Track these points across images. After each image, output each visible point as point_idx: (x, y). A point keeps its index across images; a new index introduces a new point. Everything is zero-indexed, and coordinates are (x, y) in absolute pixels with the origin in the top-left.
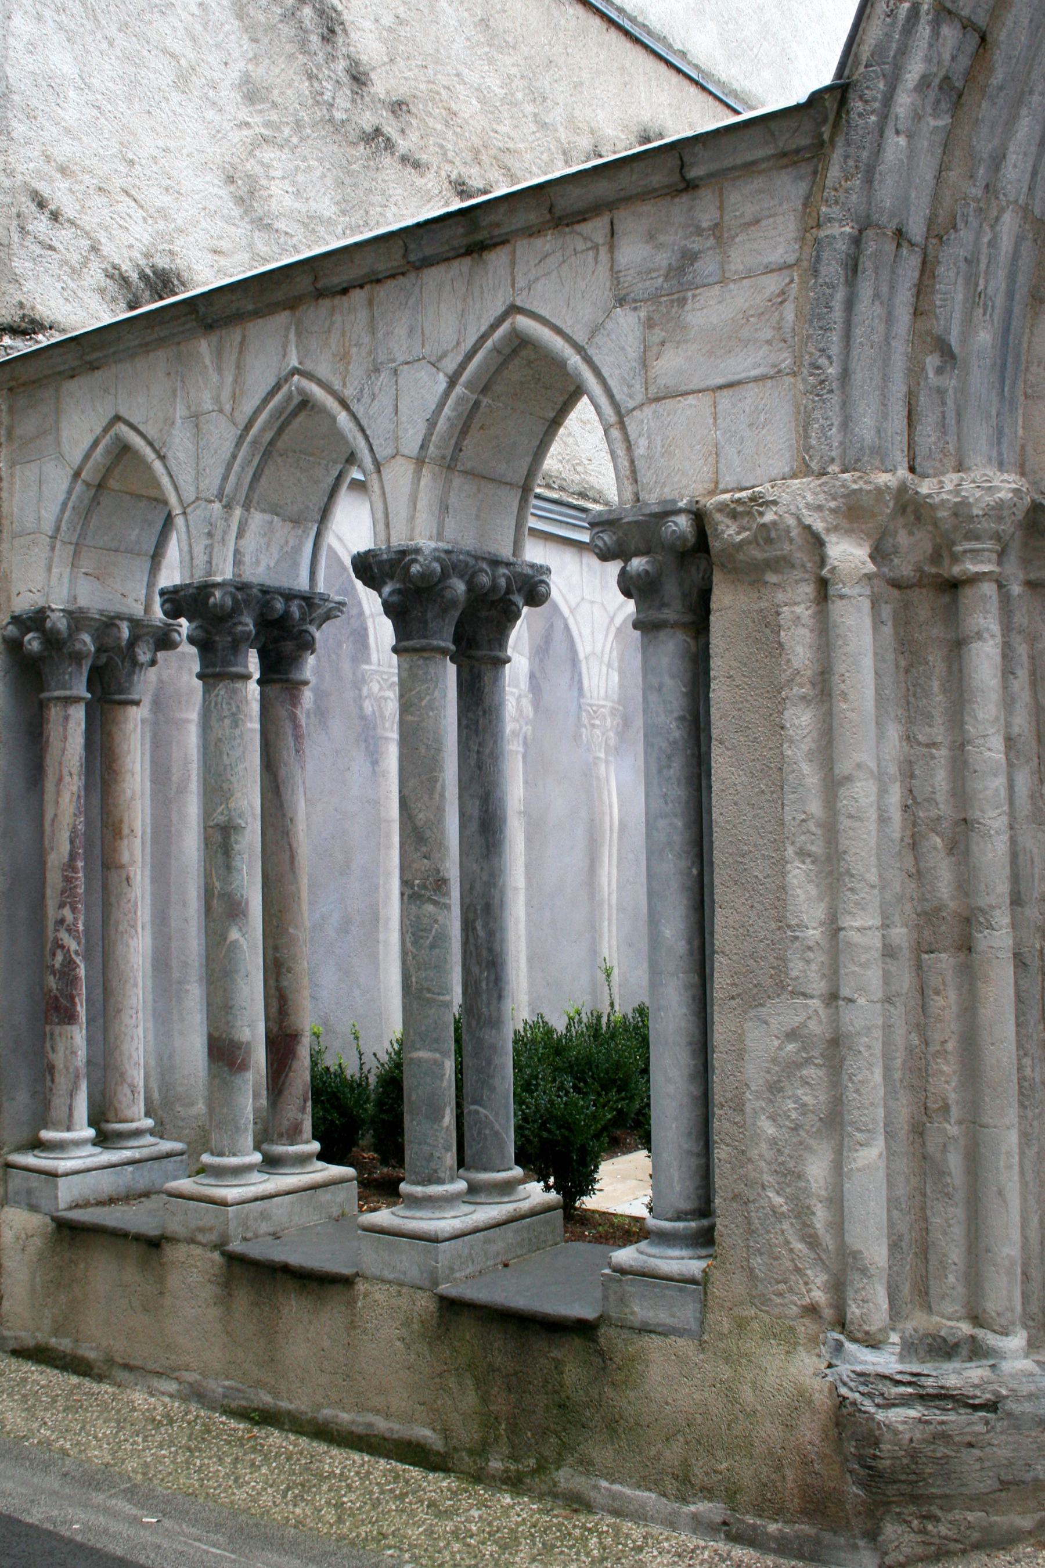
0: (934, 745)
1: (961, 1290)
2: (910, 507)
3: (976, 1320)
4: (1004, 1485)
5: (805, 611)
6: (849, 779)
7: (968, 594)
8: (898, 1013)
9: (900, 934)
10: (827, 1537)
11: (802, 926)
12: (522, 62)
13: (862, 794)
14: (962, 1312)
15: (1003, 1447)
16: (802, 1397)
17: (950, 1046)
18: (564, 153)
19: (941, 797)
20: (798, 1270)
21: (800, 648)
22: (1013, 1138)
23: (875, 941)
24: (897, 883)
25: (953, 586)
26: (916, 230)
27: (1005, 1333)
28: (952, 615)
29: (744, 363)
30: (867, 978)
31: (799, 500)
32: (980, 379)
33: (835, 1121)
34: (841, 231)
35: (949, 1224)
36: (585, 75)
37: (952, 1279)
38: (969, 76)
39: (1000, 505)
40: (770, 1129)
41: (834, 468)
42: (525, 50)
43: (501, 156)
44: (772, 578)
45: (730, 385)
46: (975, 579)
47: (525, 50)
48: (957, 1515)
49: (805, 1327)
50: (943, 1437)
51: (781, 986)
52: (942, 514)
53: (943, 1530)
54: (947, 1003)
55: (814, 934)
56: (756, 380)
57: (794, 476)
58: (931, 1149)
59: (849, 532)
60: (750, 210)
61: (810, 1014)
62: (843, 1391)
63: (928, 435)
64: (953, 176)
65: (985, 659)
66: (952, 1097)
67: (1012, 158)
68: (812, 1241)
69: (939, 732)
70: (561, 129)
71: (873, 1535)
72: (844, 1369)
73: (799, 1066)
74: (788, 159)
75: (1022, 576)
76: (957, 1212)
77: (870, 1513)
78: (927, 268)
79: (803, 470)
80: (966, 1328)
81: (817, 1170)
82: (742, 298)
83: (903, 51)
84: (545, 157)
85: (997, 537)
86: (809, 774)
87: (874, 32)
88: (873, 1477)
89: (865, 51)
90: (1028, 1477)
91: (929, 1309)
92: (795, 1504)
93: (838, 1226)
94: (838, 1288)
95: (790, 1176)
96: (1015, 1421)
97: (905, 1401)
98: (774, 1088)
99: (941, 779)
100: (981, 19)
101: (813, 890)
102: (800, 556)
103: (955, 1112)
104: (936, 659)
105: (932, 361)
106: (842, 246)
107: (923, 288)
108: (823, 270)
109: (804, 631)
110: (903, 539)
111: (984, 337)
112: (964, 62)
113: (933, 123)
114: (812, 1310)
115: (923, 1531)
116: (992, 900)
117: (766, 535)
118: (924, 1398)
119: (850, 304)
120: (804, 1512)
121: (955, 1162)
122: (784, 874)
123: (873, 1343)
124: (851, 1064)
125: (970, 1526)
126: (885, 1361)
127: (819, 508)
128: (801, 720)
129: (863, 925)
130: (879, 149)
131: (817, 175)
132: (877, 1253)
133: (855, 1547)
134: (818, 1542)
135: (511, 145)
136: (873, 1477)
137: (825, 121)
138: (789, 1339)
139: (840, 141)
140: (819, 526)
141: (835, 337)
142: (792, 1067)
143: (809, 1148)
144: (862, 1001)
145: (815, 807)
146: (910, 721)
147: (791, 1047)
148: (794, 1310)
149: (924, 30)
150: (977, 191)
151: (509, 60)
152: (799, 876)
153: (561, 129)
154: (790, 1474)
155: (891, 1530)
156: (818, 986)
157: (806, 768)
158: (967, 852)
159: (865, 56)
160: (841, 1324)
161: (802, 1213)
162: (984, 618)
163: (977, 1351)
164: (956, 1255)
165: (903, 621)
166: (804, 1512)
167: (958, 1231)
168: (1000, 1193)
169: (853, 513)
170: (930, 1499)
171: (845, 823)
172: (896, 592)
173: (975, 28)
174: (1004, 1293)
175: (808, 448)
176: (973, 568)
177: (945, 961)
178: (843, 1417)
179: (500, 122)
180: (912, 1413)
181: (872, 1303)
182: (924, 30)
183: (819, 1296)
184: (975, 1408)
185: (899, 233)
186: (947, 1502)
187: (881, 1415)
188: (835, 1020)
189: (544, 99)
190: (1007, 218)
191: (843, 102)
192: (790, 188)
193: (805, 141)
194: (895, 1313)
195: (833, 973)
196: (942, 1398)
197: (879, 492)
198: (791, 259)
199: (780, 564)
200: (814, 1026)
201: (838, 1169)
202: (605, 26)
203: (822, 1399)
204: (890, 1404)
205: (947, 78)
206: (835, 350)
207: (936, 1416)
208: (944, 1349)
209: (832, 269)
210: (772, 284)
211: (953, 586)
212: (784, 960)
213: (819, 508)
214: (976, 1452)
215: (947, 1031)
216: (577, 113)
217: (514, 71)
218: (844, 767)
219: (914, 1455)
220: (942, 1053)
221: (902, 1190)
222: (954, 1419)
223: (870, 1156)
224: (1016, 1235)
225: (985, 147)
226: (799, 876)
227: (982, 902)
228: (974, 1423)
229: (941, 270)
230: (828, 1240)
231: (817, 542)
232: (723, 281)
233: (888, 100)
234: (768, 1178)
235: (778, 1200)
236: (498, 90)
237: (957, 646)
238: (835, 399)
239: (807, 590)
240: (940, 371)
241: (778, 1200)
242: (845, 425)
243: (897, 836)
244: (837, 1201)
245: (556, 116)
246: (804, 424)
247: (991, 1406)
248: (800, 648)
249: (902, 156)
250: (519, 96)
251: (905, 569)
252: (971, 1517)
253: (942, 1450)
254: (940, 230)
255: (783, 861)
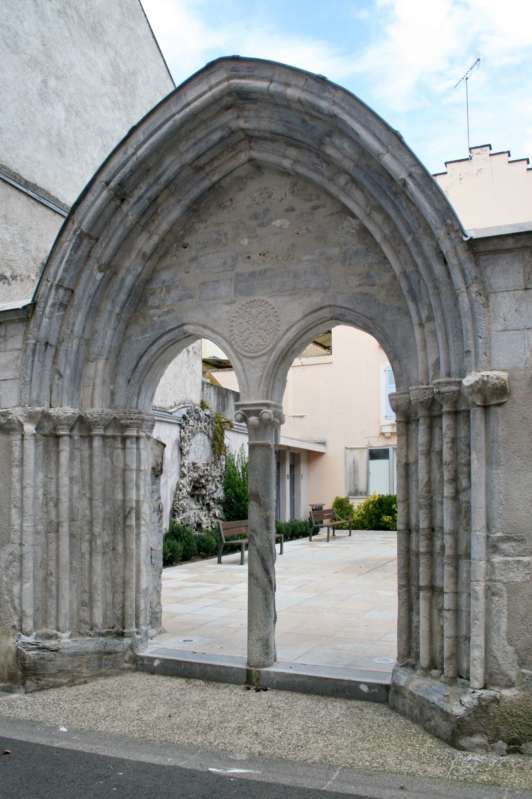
0: (52, 478)
1: (55, 622)
2: (46, 416)
3: (58, 630)
4: (60, 671)
5: (18, 442)
6: (25, 487)
7: (61, 440)
8: (39, 549)
9: (40, 528)
10: (13, 685)
11: (14, 525)
12: (19, 229)
13: (29, 491)
14: (55, 627)
15: (59, 661)
16: (9, 649)
17: (53, 558)
18: (34, 260)
19: (53, 493)
20: (11, 616)
21: (17, 453)
22: (67, 582)
23: (31, 530)
24: (40, 514)
25: (58, 437)
26: (53, 341)
27: (63, 633)
28: (57, 444)
29: (9, 375)
30: (29, 539)
31: (17, 414)
32: (66, 382)
33: (21, 577)
34: (32, 342)
35: (52, 603)
36: (44, 232)
37: (52, 619)
38: (69, 301)
39: (68, 417)
40: (5, 579)
41: (26, 405)
42: (20, 224)
43: (8, 262)
44: (12, 433)
45: (5, 380)
46: (62, 436)
47: (20, 224)
48: (46, 679)
49: (12, 631)
50: (43, 658)
51: (9, 541)
52: (54, 418)
53: (43, 683)
54: (53, 546)
55: (17, 527)
56: (11, 379)
57: (17, 406)
58: (48, 585)
59: (30, 422)
60: (12, 333)
61: (14, 548)
62: (19, 647)
63: (54, 397)
64: (64, 327)
65: (64, 456)
66: (53, 571)
67: (77, 325)
68: (15, 608)
69: (53, 475)
70: (33, 251)
71: (24, 684)
72: (20, 642)
73: (13, 562)
74: (21, 320)
75: (78, 434)
76: (55, 601)
77: (23, 678)
78: (57, 351)
79: (19, 405)
80: (55, 632)
81: (16, 590)
82: (352, 168)
83: (49, 296)
84: (26, 262)
85: (68, 425)
86: (17, 486)
87: (43, 289)
88: (24, 669)
89: (40, 293)
90: (66, 669)
91: (47, 627)
92: (6, 678)
93: (21, 604)
94: (21, 620)
95: (10, 591)
96: (63, 655)
97: (34, 649)
98: (7, 568)
99: (53, 488)
100: (71, 287)
101: (17, 516)
102: (17, 428)
103: (54, 575)
104: (53, 455)
105: (57, 376)
106: (32, 346)
107: (55, 357)
108: (28, 352)
109: (18, 448)
110: (46, 424)
111: (68, 372)
112: (67, 298)
113: (57, 314)
114: (14, 627)
115: (37, 683)
116: (63, 520)
117: (10, 422)
118: (39, 648)
119: (33, 361)
120: (8, 680)
121: (54, 588)
122: (10, 511)
123: (28, 635)
124: (24, 561)
125: (50, 682)
126: (30, 639)
127: (22, 416)
128: (16, 471)
129: (28, 525)
130: (41, 322)
131: (28, 326)
132: (29, 611)
133: (19, 688)
134: (11, 687)
135: (13, 258)
136: (24, 669)
137: (29, 312)
138: (8, 635)
139: (33, 317)
140: (22, 420)
141: (29, 370)
142: (11, 562)
143: (14, 584)
144: (26, 545)
145: (18, 494)
146: (47, 472)
147: (11, 557)
148: (10, 627)
149: (53, 291)
150: (69, 332)
151: (14, 229)
152: (14, 512)
153: (33, 251)
154: (6, 670)
155: (28, 683)
156: (18, 541)
157: (16, 484)
158: (58, 507)
159: (40, 296)
160: (21, 630)
161: (12, 601)
162: (65, 446)
163: (56, 637)
164: (53, 612)
165: (46, 446)
166: (8, 680)
167: (54, 606)
168: (63, 596)
169: (31, 417)
170: (39, 674)
171: (24, 499)
172: (44, 438)
173: (69, 289)
174: (64, 622)
175: (21, 399)
176: (62, 433)
177: (52, 535)
178: (18, 654)
179: (8, 250)
180: (35, 652)
181: (29, 624)
182: (53, 291)
183: (16, 623)
184: (52, 651)
185: (47, 344)
186: (44, 675)
187: (27, 653)
188: (21, 550)
189: (27, 241)
190: (75, 341)
191: (34, 307)
192: (21, 327)
193: (25, 317)
194: (36, 626)
195: (21, 538)
196: (44, 648)
197: (37, 413)
198: (20, 348)
199: (13, 430)
200: (16, 552)
201: (21, 590)
202: (54, 214)
203: (14, 650)
204: (30, 650)
205: (61, 303)
206: (28, 374)
207: (42, 653)
208: (49, 637)
209: (29, 352)
210: (16, 354)
211: (58, 437)
212: (9, 534)
213: (22, 416)
214: (52, 662)
215: (52, 553)
216: (40, 245)
217: (15, 232)
218: (25, 484)
219: (35, 663)
220: (51, 559)
221: (39, 595)
222: (46, 654)
223: (28, 585)
224: (67, 607)
225: (71, 322)
226: (14, 512)
227: (61, 520)
228: (51, 655)
229: (60, 352)
230: (18, 608)
231: (22, 425)
232: (5, 351)
233: (45, 308)
234: (5, 592)
235: (7, 598)
236: (8, 239)
237: (58, 453)
238: (28, 387)
239: (19, 437)
240: (58, 379)
241: (7, 598)
242: (30, 394)
243: (41, 502)
244: (20, 598)
245: (32, 247)
246: (21, 392)
247: (56, 651)
248: (17, 453)
249: (46, 323)
250: (17, 241)
251: (46, 431)
252: (50, 679)
253: (43, 662)
254: (60, 342)
255: (10, 508)
